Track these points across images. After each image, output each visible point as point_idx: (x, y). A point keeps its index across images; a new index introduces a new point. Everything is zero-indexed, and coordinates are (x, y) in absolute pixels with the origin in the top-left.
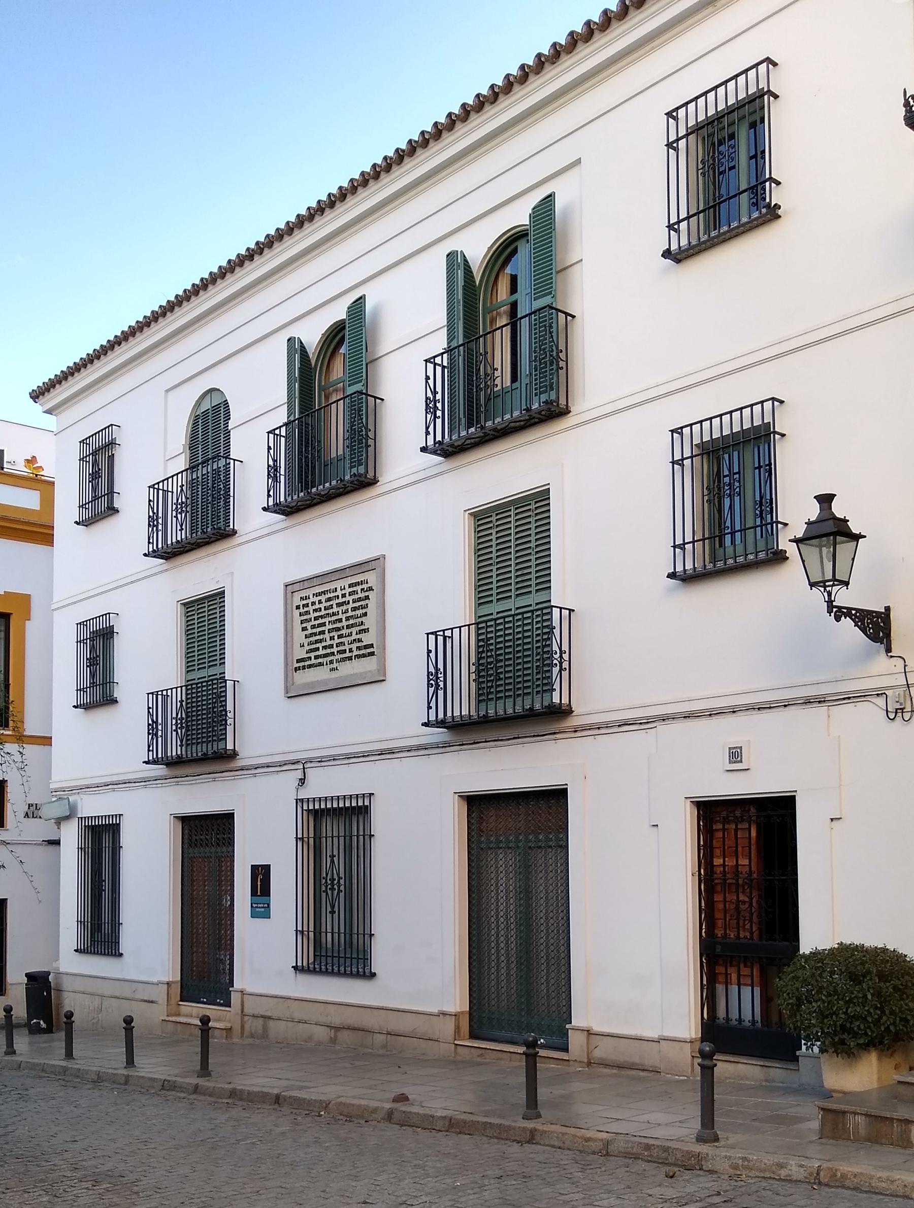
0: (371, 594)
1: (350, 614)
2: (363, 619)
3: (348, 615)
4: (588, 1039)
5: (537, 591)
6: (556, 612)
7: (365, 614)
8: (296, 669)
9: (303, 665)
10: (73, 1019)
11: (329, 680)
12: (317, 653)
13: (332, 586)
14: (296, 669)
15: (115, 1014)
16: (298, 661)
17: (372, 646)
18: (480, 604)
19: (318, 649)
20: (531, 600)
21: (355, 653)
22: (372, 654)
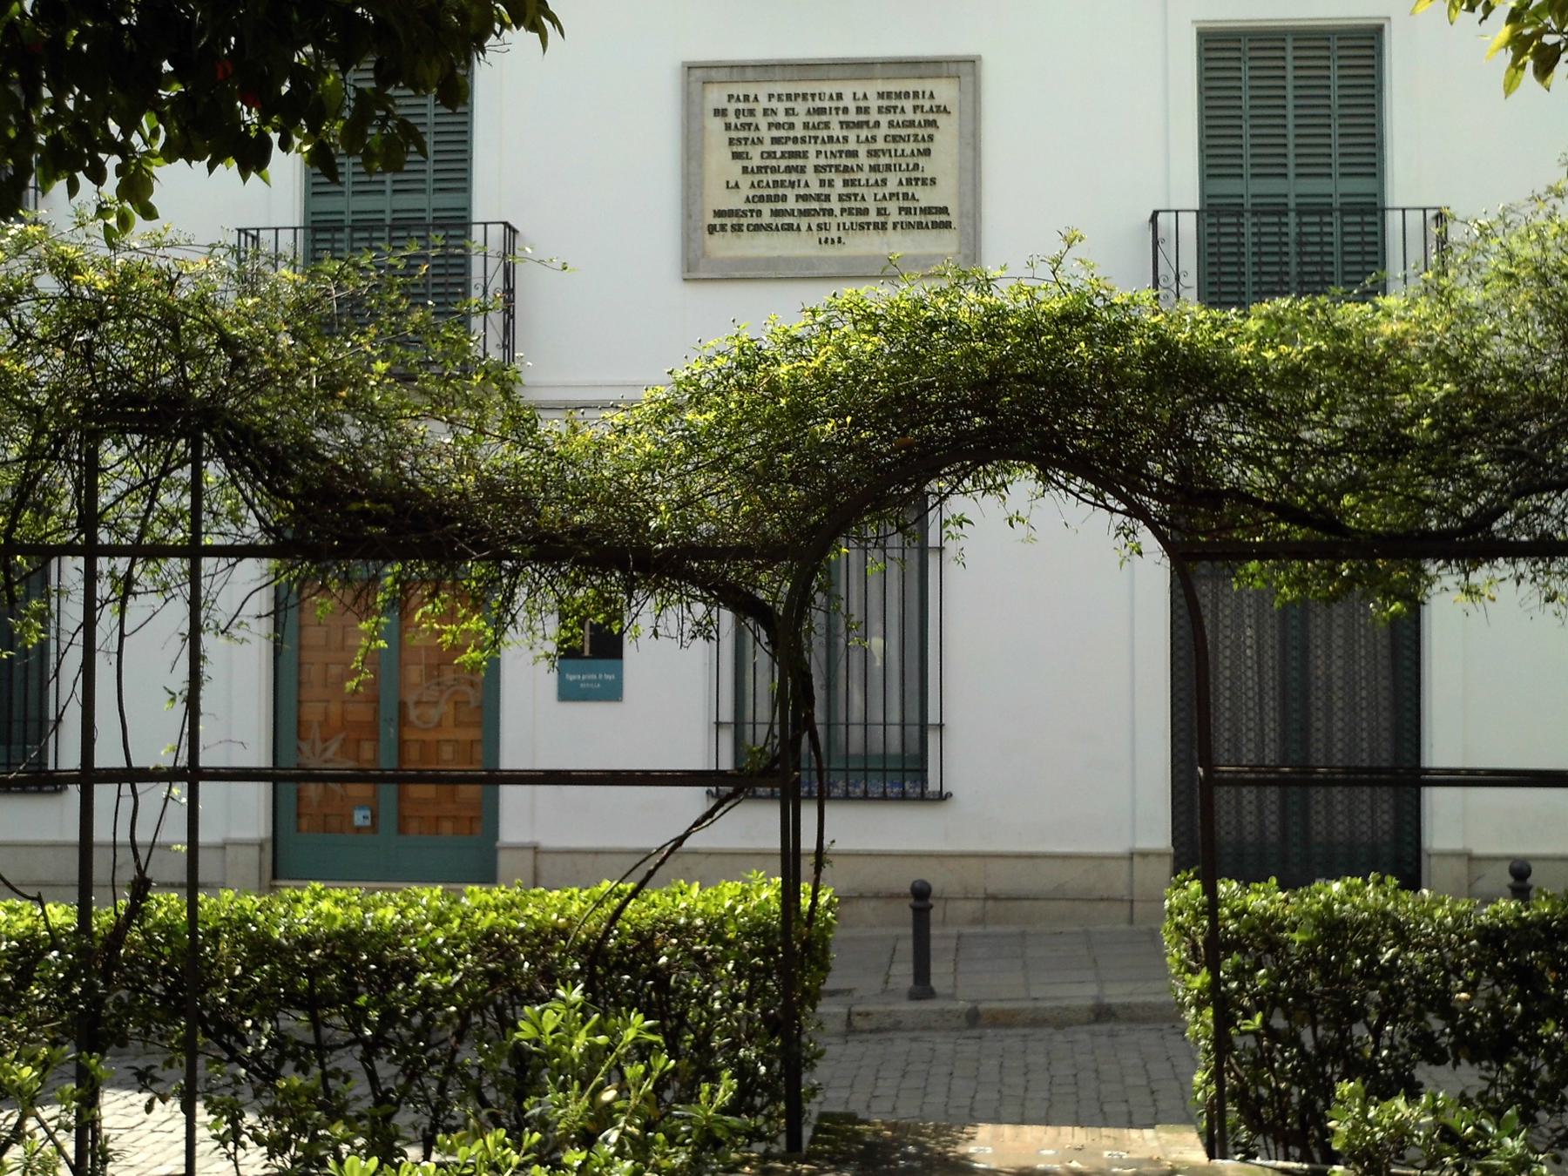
0: (941, 119)
1: (880, 145)
2: (922, 161)
3: (874, 146)
4: (535, 859)
5: (435, 190)
6: (477, 232)
7: (927, 152)
8: (712, 229)
9: (729, 221)
10: (1530, 881)
11: (822, 259)
12: (780, 206)
13: (751, 90)
14: (712, 229)
15: (902, 879)
16: (719, 214)
17: (944, 210)
18: (1209, 176)
19: (784, 198)
20: (1339, 188)
21: (894, 217)
22: (947, 225)
